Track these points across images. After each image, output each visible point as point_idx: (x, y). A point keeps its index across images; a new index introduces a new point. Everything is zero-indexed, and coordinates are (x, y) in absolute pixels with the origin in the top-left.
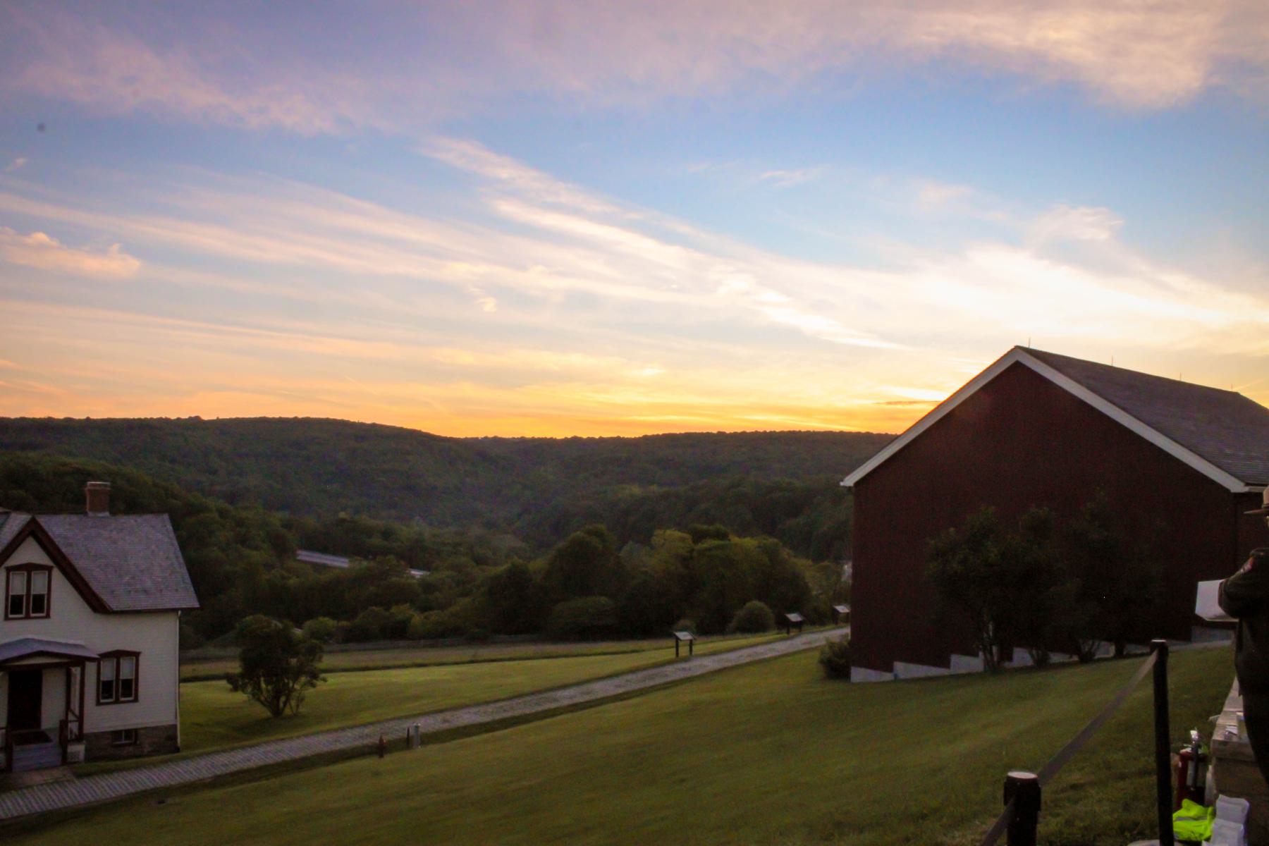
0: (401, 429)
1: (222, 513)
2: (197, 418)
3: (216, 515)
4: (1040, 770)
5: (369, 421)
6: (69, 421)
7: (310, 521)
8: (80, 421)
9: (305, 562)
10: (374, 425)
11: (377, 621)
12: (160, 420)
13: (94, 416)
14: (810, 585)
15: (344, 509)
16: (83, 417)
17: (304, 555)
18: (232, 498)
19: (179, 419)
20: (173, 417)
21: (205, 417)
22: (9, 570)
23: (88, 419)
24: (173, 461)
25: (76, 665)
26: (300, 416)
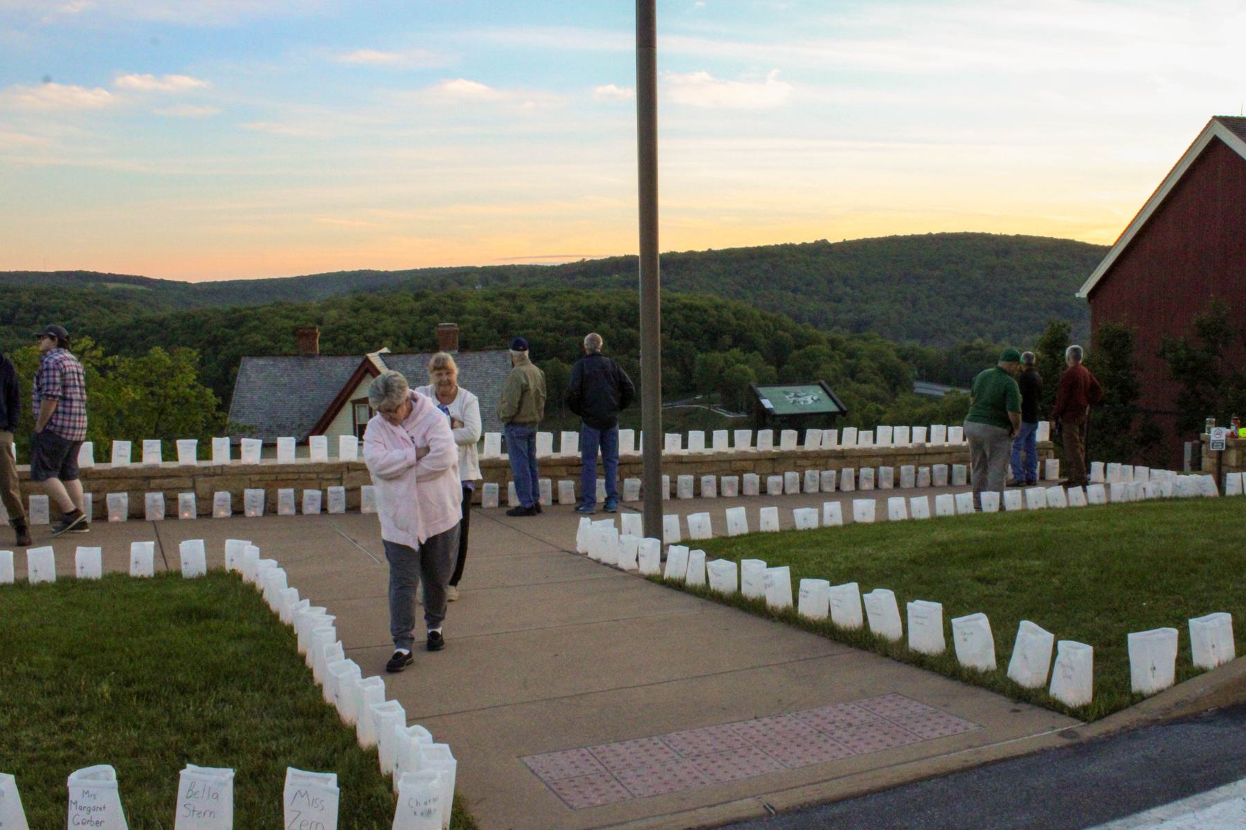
0: (1052, 240)
1: (834, 344)
2: (824, 241)
3: (825, 348)
4: (340, 771)
5: (382, 269)
6: (691, 254)
7: (935, 350)
8: (702, 254)
9: (922, 395)
10: (1018, 236)
11: (154, 478)
12: (785, 247)
13: (715, 248)
14: (1182, 476)
15: (981, 335)
16: (706, 249)
17: (922, 388)
18: (859, 327)
19: (804, 244)
20: (798, 243)
21: (831, 241)
22: (355, 402)
23: (710, 251)
24: (795, 291)
25: (286, 483)
26: (834, 238)
